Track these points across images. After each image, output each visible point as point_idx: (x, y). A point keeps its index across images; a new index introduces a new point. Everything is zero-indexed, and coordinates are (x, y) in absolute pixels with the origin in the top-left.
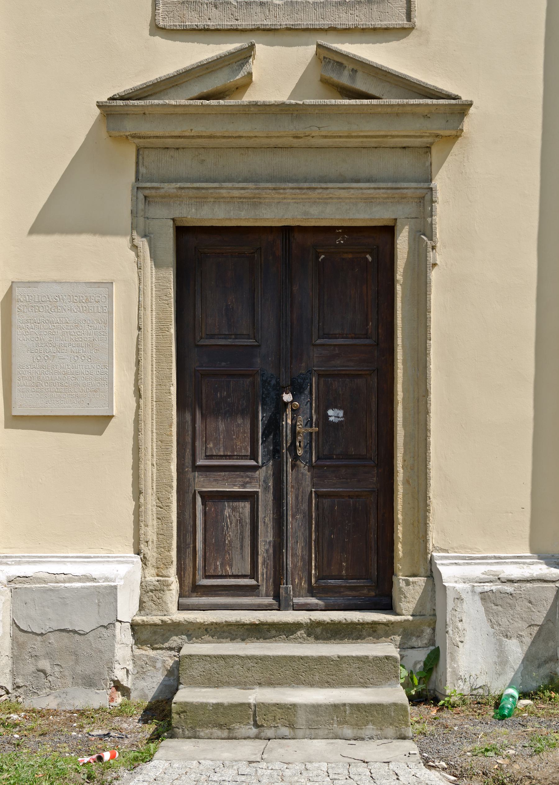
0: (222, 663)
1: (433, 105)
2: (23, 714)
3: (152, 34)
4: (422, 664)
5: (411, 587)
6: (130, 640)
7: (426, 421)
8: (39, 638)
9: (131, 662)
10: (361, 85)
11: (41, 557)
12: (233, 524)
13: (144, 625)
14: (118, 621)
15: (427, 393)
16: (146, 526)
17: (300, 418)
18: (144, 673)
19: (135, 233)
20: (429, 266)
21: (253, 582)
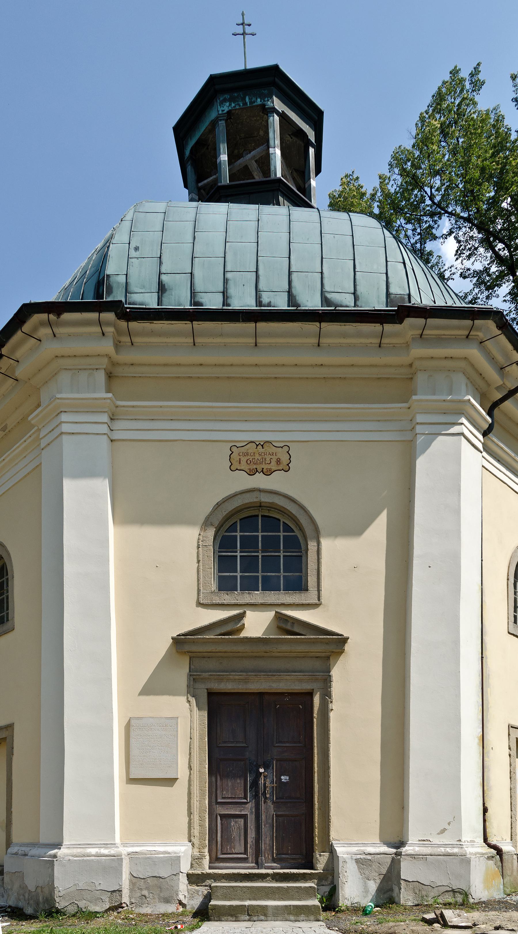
0: (232, 889)
1: (330, 638)
2: (135, 915)
3: (197, 606)
4: (328, 893)
5: (322, 857)
6: (187, 882)
7: (329, 781)
8: (143, 880)
9: (187, 892)
10: (296, 629)
11: (143, 843)
12: (236, 829)
13: (193, 875)
14: (181, 872)
15: (329, 768)
16: (194, 829)
17: (268, 780)
18: (193, 897)
19: (189, 695)
20: (329, 710)
21: (245, 856)
